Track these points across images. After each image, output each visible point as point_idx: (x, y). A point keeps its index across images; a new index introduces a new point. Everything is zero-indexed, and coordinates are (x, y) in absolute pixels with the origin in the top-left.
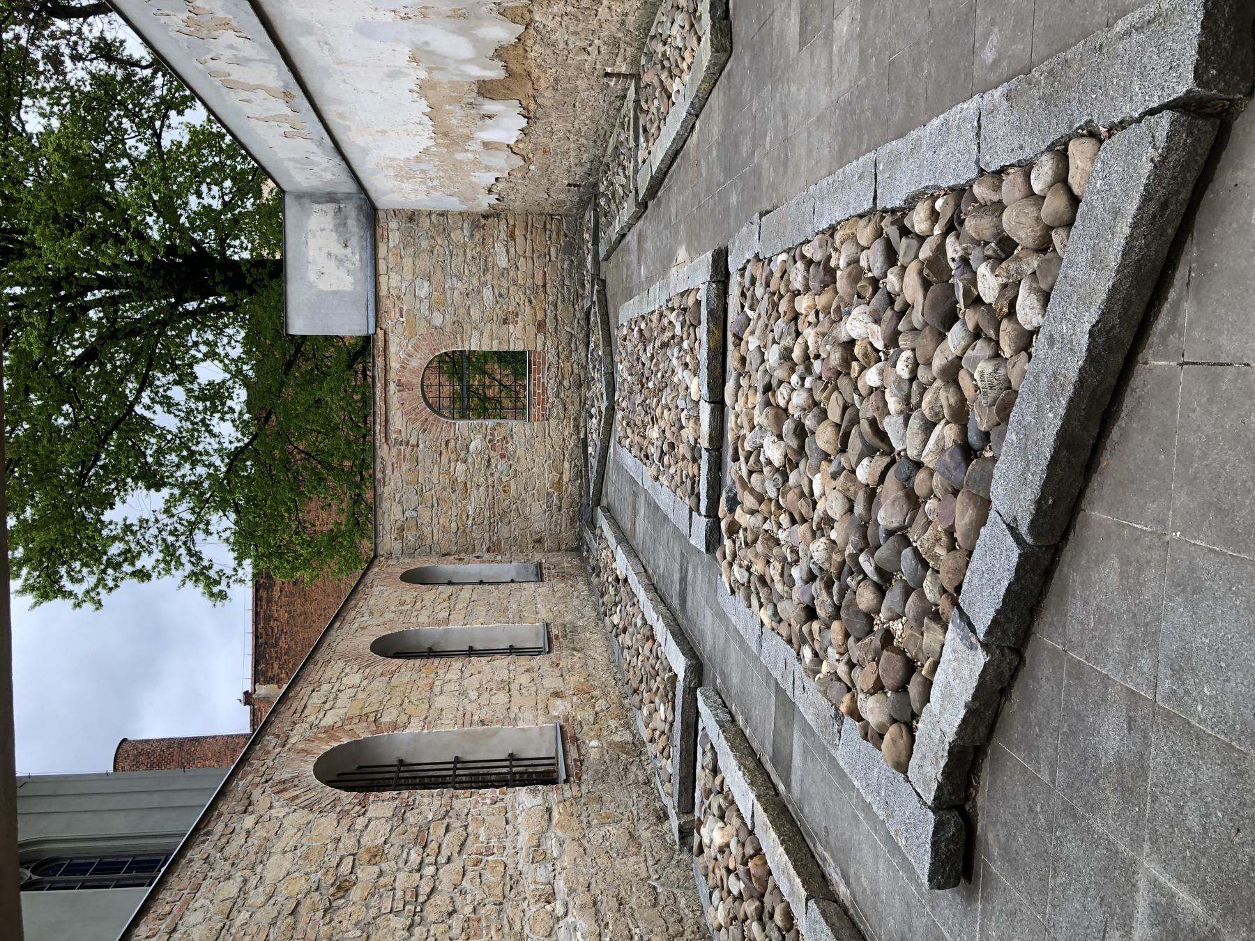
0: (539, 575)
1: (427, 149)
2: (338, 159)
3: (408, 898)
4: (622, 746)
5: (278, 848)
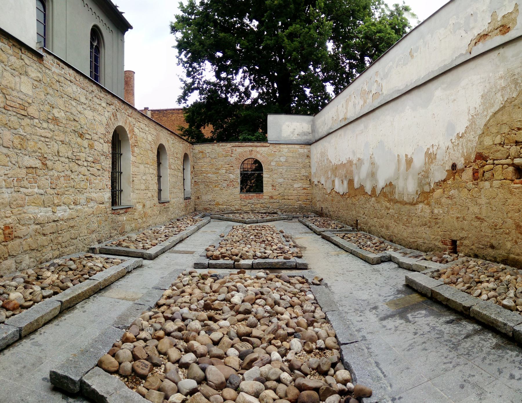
1: (331, 162)
2: (326, 133)
5: (95, 114)
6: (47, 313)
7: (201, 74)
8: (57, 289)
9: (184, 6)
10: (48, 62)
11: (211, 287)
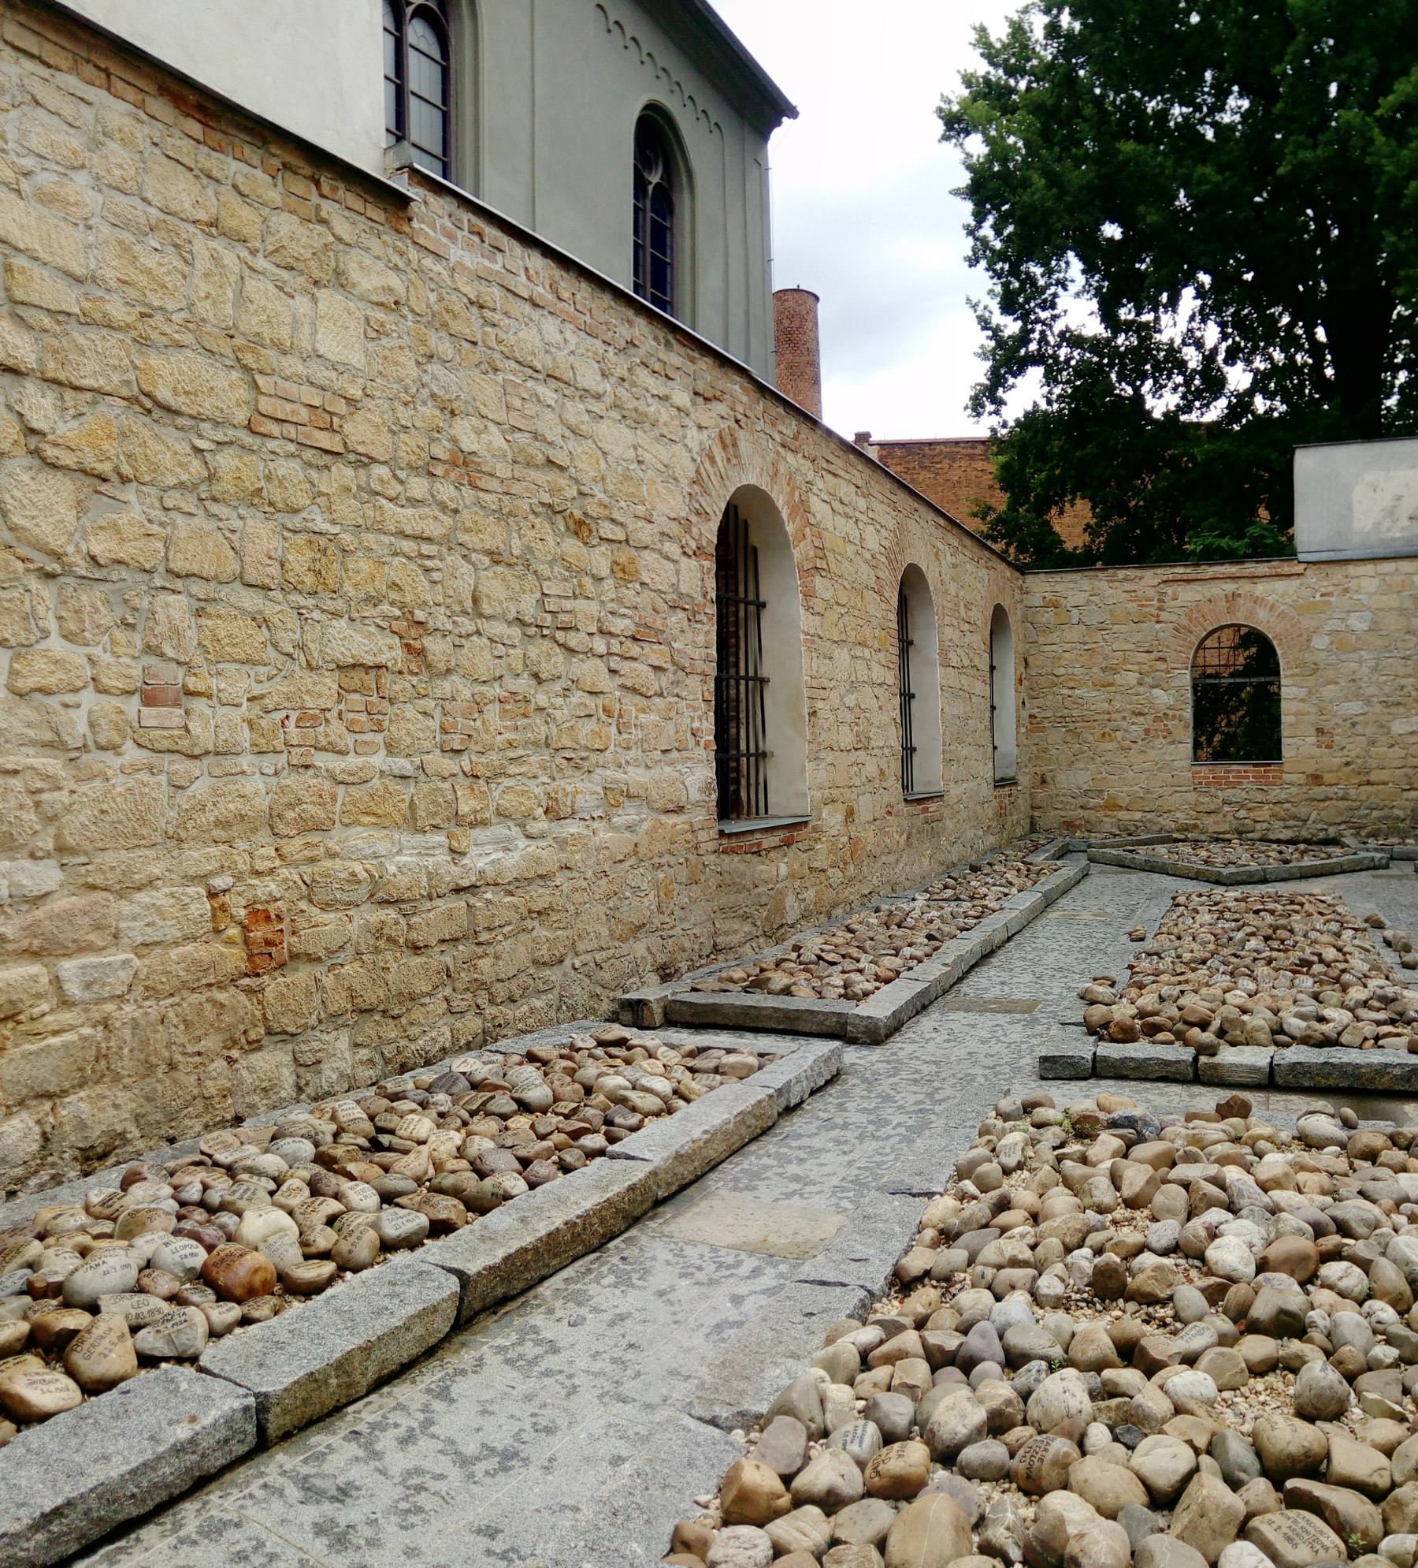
0: (1003, 783)
3: (561, 616)
4: (780, 909)
5: (642, 438)
6: (393, 1334)
7: (1053, 306)
8: (447, 1208)
9: (993, 39)
10: (433, 227)
11: (1115, 1180)
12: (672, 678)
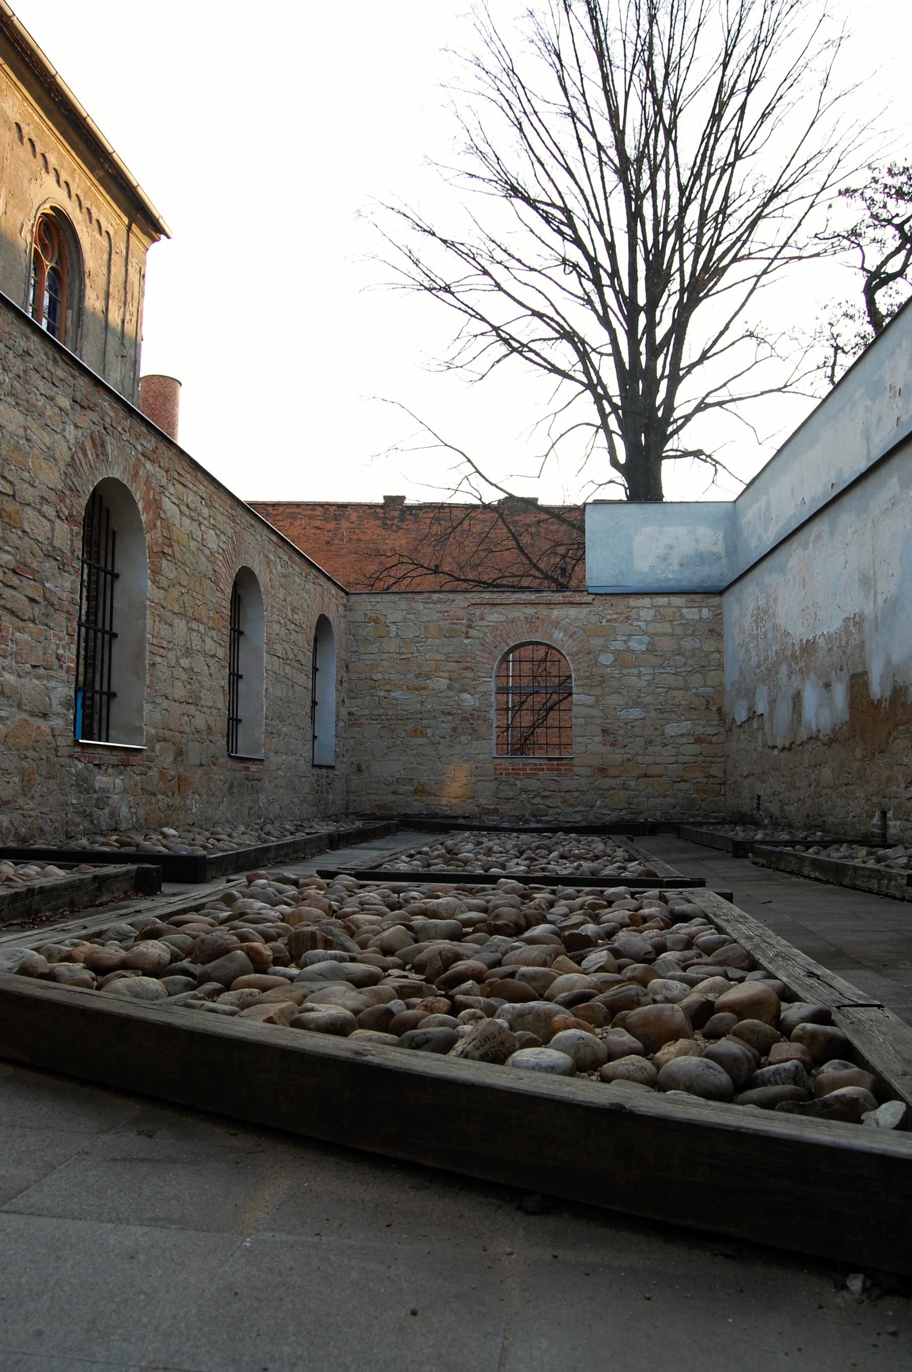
5: (30, 422)
12: (43, 610)
